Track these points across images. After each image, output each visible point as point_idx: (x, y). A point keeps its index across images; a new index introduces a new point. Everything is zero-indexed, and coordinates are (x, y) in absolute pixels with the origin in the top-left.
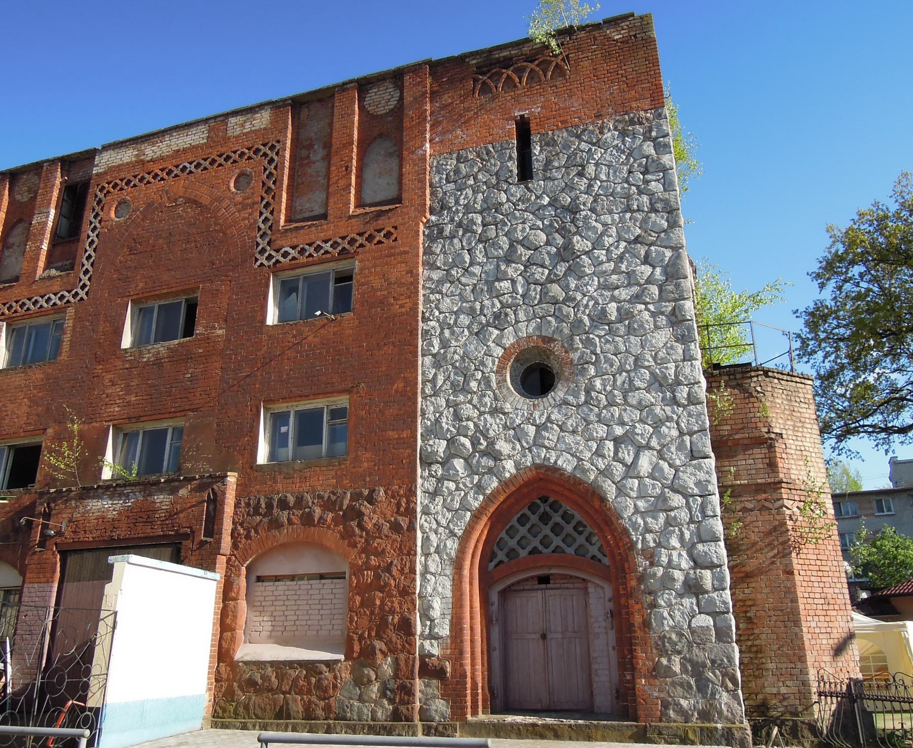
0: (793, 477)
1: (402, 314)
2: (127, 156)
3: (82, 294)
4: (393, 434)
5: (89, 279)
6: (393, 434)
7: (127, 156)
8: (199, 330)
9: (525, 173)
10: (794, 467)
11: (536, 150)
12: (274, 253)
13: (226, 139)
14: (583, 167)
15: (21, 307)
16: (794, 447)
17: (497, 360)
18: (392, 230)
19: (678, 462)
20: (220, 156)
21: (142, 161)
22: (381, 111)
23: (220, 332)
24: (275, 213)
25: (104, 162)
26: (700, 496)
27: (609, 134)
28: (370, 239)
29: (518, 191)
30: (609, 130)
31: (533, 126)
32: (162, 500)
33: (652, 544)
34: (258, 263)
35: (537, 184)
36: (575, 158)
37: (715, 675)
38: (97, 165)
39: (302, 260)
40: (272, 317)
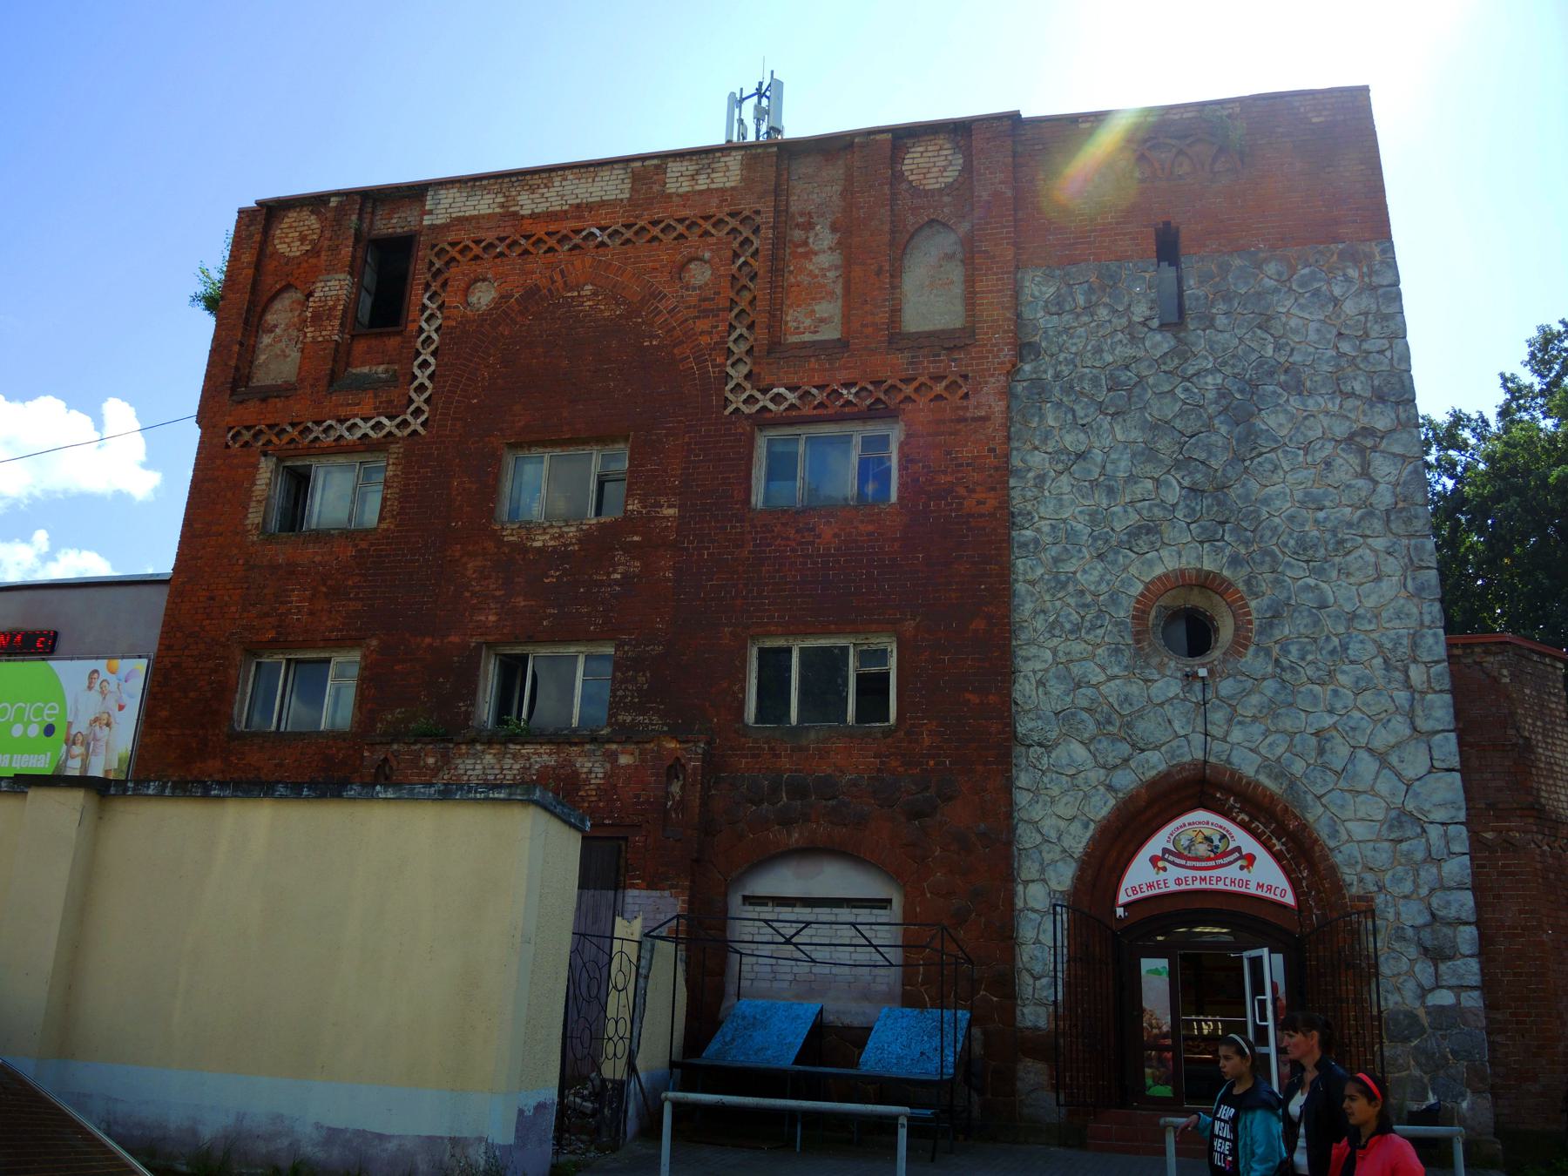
2: (484, 204)
4: (974, 699)
15: (326, 431)
21: (515, 214)
22: (931, 184)
23: (671, 511)
26: (1443, 824)
29: (1161, 343)
38: (430, 212)
39: (807, 411)
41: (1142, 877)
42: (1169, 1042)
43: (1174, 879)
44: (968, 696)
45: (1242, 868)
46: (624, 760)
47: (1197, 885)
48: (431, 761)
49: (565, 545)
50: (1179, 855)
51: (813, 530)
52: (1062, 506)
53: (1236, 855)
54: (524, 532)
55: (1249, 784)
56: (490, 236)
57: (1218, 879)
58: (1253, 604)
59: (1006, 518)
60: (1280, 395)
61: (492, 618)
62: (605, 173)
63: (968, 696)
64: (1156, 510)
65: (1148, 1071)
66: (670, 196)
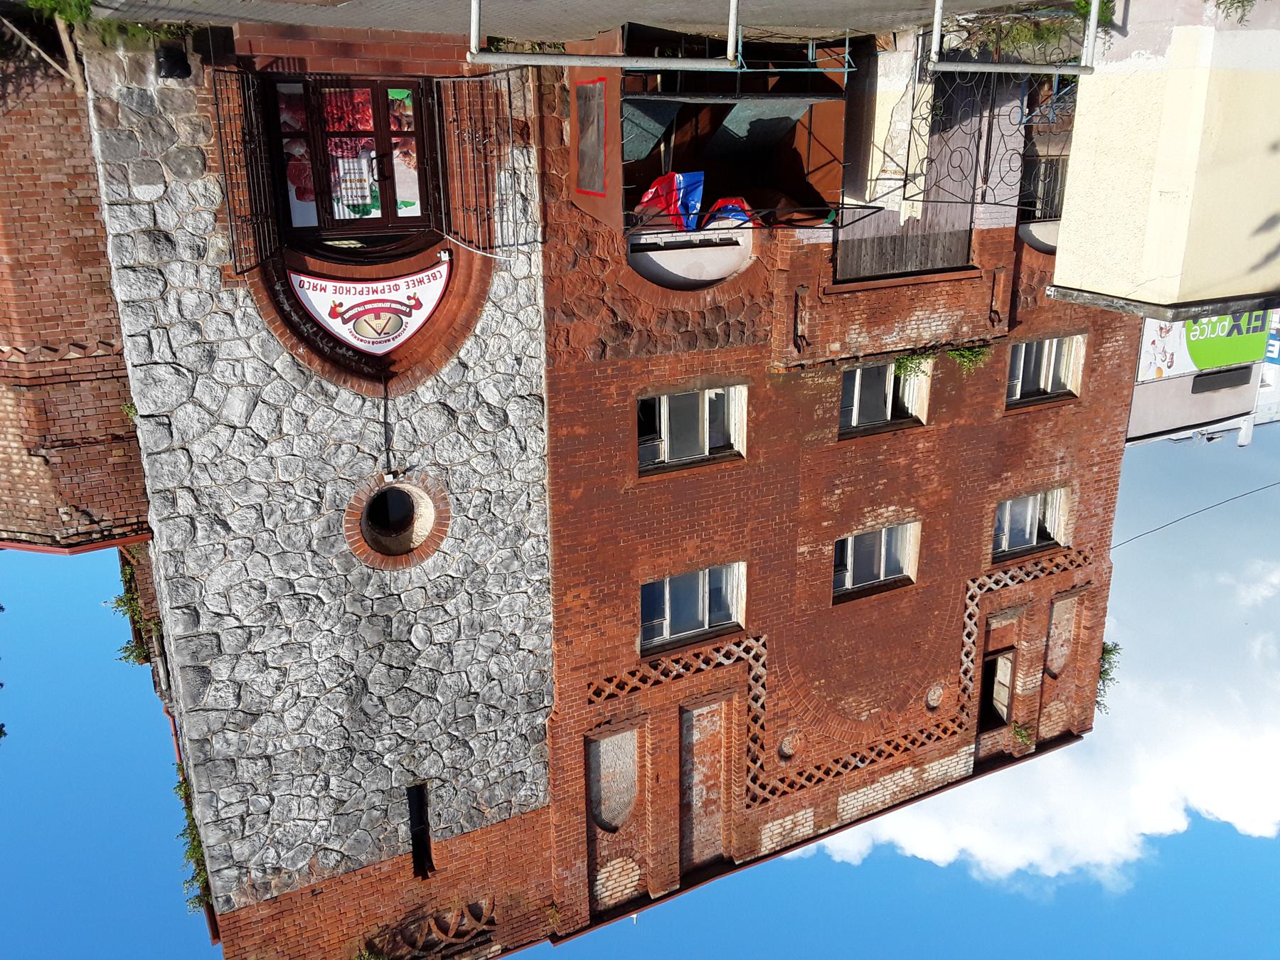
0: (11, 395)
1: (576, 586)
2: (935, 770)
3: (974, 589)
4: (579, 430)
5: (966, 607)
6: (579, 430)
7: (935, 770)
8: (829, 550)
9: (418, 797)
10: (10, 409)
11: (404, 830)
12: (744, 655)
13: (815, 805)
14: (335, 813)
16: (10, 437)
17: (449, 534)
18: (594, 698)
19: (190, 407)
20: (820, 780)
21: (915, 766)
24: (746, 708)
25: (961, 762)
26: (156, 363)
27: (300, 865)
28: (621, 686)
29: (429, 768)
30: (299, 871)
31: (409, 864)
32: (859, 339)
33: (224, 295)
34: (762, 641)
35: (399, 781)
36: (347, 825)
37: (128, 119)
38: (970, 754)
39: (707, 649)
40: (737, 578)
41: (426, 289)
42: (394, 140)
43: (399, 290)
44: (583, 431)
45: (341, 305)
46: (836, 346)
47: (380, 285)
48: (965, 329)
49: (873, 510)
50: (396, 312)
51: (702, 552)
52: (510, 606)
53: (346, 316)
54: (901, 516)
55: (345, 382)
56: (931, 744)
57: (361, 293)
58: (346, 547)
59: (561, 587)
60: (325, 742)
61: (920, 446)
62: (855, 813)
63: (583, 431)
64: (433, 616)
65: (410, 113)
66: (811, 805)
